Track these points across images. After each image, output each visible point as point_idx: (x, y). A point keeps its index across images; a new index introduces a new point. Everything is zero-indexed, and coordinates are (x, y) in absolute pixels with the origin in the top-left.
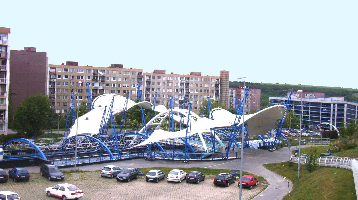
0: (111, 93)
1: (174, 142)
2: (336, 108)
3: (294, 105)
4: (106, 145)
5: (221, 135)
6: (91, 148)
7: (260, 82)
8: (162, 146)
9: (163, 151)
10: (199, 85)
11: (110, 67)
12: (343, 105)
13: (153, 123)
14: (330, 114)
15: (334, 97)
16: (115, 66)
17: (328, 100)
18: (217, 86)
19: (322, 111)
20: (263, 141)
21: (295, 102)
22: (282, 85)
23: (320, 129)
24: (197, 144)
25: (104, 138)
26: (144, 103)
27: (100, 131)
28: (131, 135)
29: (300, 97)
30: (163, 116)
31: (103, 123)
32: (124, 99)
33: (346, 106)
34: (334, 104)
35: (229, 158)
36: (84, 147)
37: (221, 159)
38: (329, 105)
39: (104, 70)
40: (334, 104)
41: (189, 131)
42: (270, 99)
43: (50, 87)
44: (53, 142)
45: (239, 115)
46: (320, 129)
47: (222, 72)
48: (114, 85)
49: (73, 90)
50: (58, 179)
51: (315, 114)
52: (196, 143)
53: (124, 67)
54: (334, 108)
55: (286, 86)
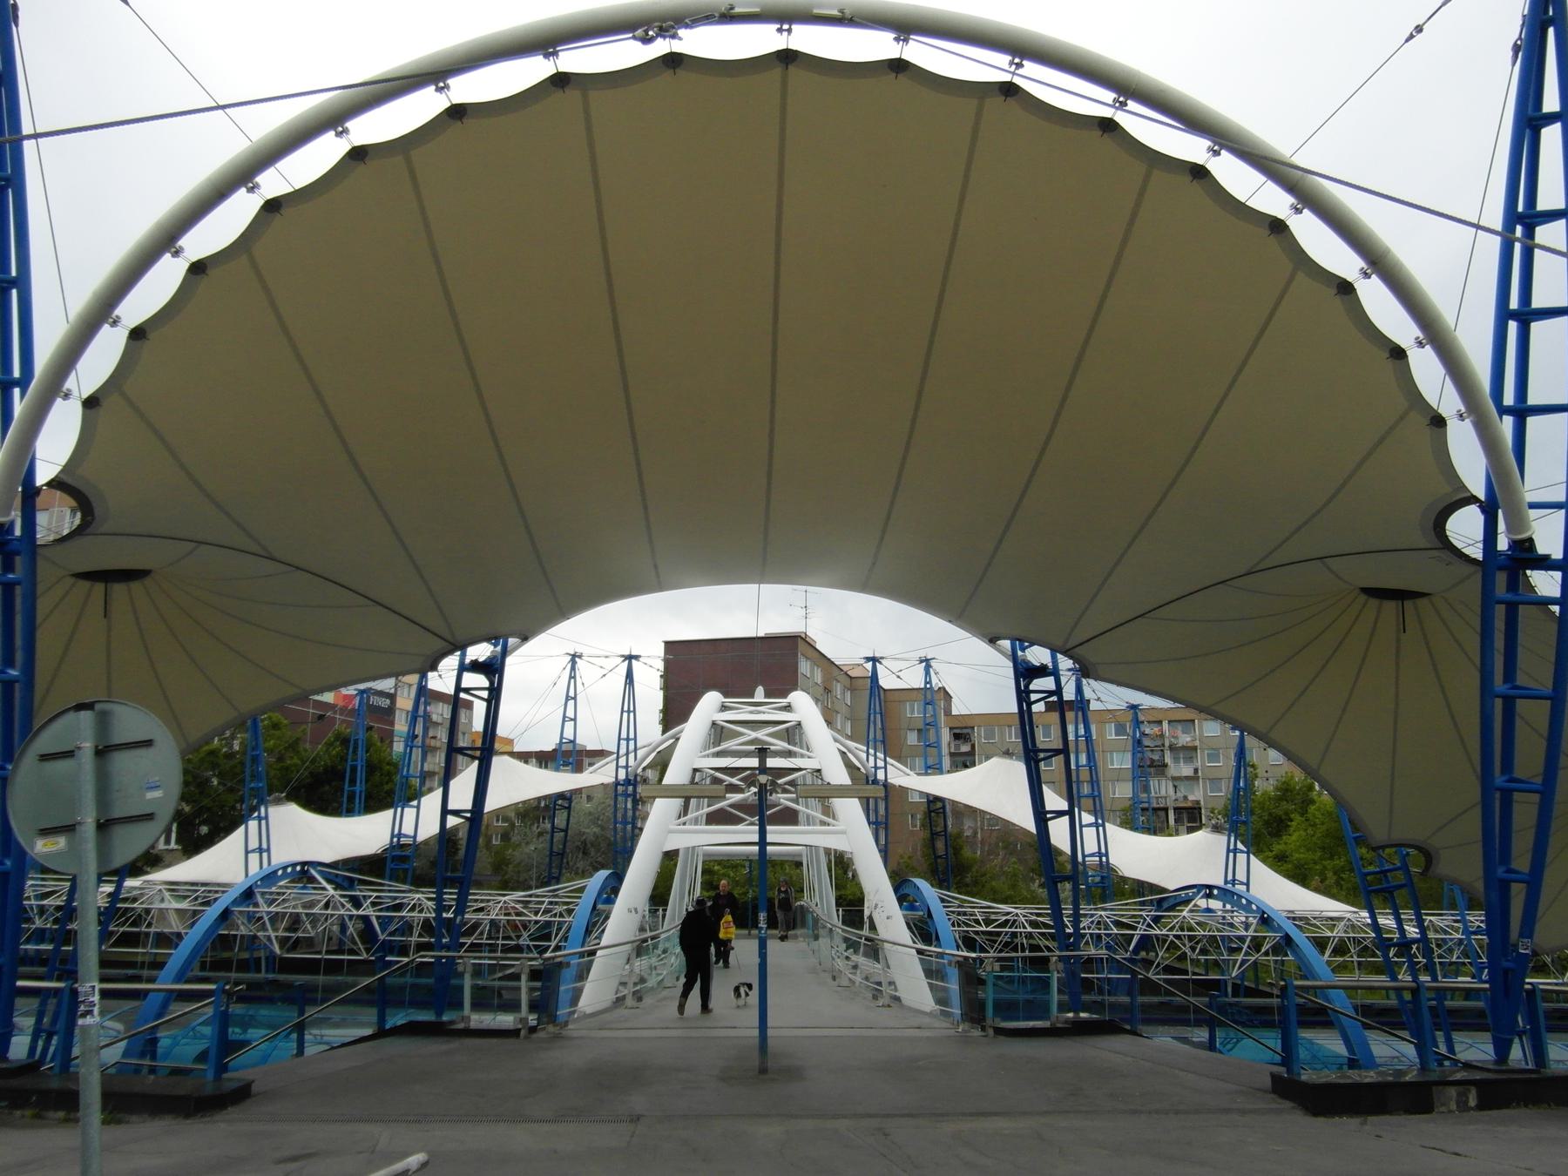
8: (576, 981)
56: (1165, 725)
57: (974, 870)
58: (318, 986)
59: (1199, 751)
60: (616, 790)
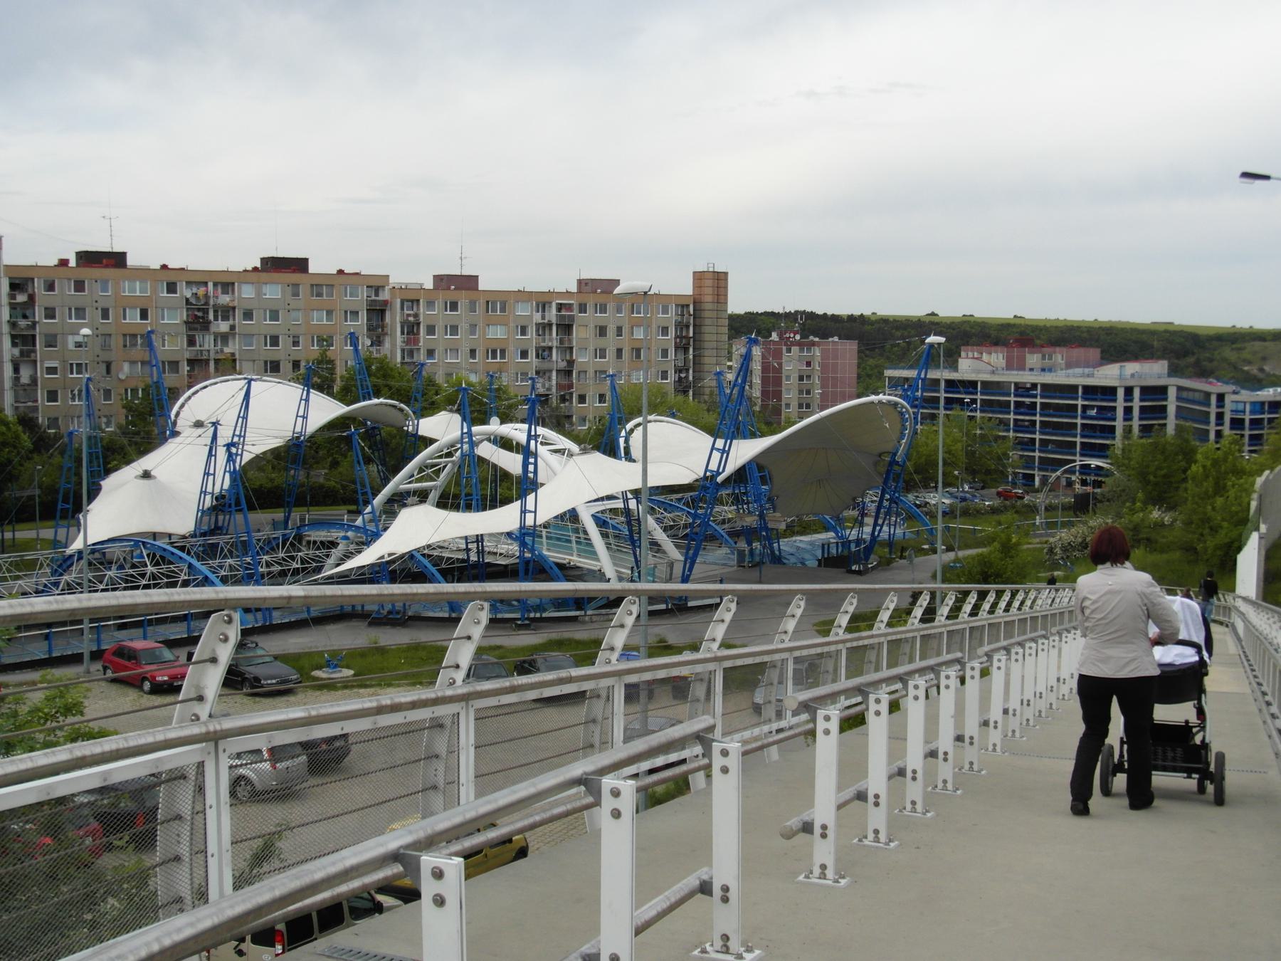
0: (266, 371)
1: (481, 552)
2: (1136, 404)
3: (979, 397)
5: (674, 521)
7: (867, 312)
8: (440, 571)
10: (611, 331)
11: (255, 269)
12: (1162, 391)
13: (410, 483)
14: (1114, 427)
15: (1127, 360)
16: (274, 265)
17: (1109, 375)
18: (682, 326)
19: (1083, 418)
20: (837, 534)
21: (985, 384)
23: (1077, 486)
24: (579, 556)
25: (215, 546)
26: (376, 405)
27: (198, 522)
29: (1009, 366)
30: (449, 455)
31: (209, 489)
32: (295, 391)
33: (1172, 393)
34: (1129, 391)
35: (690, 604)
37: (663, 607)
38: (1110, 392)
39: (233, 284)
40: (1129, 391)
41: (530, 506)
42: (889, 378)
44: (9, 571)
45: (723, 441)
46: (1077, 486)
47: (699, 277)
48: (275, 341)
50: (175, 684)
51: (1057, 427)
52: (575, 553)
53: (312, 269)
54: (1129, 404)
56: (210, 285)
57: (1199, 457)
58: (40, 519)
59: (237, 310)
60: (977, 358)
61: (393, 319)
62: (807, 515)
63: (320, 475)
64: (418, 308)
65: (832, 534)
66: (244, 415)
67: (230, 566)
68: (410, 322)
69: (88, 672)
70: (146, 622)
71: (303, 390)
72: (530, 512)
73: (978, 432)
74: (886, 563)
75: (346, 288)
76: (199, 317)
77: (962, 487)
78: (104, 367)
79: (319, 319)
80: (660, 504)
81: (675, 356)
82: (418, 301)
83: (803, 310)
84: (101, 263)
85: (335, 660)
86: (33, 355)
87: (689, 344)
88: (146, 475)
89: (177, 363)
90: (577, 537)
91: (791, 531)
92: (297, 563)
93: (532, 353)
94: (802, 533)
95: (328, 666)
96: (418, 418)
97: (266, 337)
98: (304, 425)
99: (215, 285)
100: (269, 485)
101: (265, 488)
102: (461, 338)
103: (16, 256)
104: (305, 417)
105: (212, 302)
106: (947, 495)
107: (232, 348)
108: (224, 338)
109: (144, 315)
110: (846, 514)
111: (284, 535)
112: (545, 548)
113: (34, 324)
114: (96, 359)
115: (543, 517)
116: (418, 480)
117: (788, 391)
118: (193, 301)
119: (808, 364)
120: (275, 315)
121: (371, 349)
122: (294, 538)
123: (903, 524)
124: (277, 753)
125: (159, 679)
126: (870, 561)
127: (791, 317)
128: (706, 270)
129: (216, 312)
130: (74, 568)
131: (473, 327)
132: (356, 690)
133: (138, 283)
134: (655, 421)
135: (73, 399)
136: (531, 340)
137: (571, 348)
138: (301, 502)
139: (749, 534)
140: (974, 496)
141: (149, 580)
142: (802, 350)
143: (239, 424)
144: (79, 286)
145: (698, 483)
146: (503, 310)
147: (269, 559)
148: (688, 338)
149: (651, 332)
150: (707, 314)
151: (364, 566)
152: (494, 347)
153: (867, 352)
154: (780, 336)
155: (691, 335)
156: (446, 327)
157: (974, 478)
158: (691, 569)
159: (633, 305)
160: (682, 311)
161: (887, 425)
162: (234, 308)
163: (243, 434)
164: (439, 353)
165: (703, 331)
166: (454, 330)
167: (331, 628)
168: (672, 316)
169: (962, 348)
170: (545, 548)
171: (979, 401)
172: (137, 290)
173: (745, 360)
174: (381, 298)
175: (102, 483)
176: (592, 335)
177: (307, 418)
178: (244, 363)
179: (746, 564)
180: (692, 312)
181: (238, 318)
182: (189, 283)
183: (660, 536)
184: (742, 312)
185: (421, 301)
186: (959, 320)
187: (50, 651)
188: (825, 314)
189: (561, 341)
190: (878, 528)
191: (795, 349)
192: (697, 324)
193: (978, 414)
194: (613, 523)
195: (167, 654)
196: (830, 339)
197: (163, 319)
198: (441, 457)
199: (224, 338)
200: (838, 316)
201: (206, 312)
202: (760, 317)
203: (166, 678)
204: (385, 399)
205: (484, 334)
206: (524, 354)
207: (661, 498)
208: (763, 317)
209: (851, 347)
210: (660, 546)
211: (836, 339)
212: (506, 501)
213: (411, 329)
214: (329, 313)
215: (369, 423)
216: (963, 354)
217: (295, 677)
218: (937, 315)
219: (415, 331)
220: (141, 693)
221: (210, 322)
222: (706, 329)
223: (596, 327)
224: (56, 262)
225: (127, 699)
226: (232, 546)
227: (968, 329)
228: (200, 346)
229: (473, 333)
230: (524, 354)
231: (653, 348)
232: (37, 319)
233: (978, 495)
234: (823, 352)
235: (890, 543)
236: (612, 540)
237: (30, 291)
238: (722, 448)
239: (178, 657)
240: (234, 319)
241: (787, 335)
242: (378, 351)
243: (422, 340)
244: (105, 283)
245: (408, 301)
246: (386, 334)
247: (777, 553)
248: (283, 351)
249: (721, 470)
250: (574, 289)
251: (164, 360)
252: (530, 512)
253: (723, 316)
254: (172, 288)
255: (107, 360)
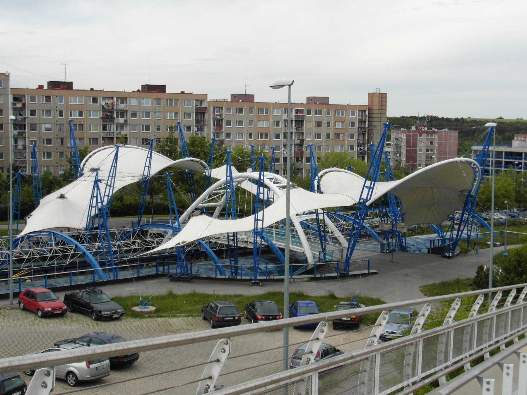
4: (88, 250)
6: (120, 251)
7: (465, 117)
8: (215, 252)
9: (215, 262)
10: (324, 125)
11: (139, 91)
16: (148, 89)
18: (362, 122)
22: (509, 122)
28: (156, 229)
35: (351, 273)
36: (126, 248)
37: (335, 274)
39: (126, 98)
42: (474, 150)
43: (14, 135)
45: (370, 182)
47: (371, 96)
48: (147, 128)
49: (62, 139)
50: (55, 313)
53: (168, 91)
55: (517, 122)
56: (115, 99)
61: (209, 117)
62: (423, 224)
63: (158, 199)
64: (222, 112)
65: (436, 235)
66: (114, 166)
67: (157, 242)
68: (218, 119)
69: (12, 304)
70: (71, 274)
71: (149, 151)
72: (260, 220)
73: (522, 180)
74: (464, 252)
75: (185, 101)
76: (109, 116)
77: (513, 210)
78: (60, 141)
79: (171, 117)
80: (341, 217)
81: (358, 138)
82: (222, 108)
83: (431, 115)
84: (60, 88)
85: (145, 301)
86: (24, 134)
87: (365, 131)
88: (62, 197)
89: (97, 139)
90: (293, 234)
91: (414, 232)
92: (154, 244)
93: (282, 135)
94: (422, 234)
95: (142, 304)
96: (211, 169)
97: (143, 126)
98: (149, 171)
99: (117, 99)
100: (135, 203)
101: (132, 204)
102: (322, 140)
103: (15, 83)
104: (149, 167)
105: (115, 108)
106: (504, 214)
107: (126, 131)
108: (122, 126)
109: (81, 114)
110: (444, 224)
111: (134, 230)
112: (275, 239)
113: (25, 118)
114: (56, 137)
115: (267, 224)
116: (208, 202)
117: (420, 158)
118: (106, 107)
119: (431, 143)
120: (148, 115)
121: (197, 132)
122: (139, 231)
123: (478, 230)
124: (90, 360)
125: (46, 309)
126: (456, 250)
127: (422, 119)
128: (375, 92)
129: (117, 113)
130: (19, 246)
131: (251, 122)
132: (155, 319)
133: (78, 97)
134: (335, 171)
135: (44, 157)
136: (281, 128)
137: (303, 133)
138: (147, 212)
139: (385, 234)
140: (519, 215)
141: (97, 250)
142: (428, 136)
143: (112, 170)
144: (48, 99)
145: (356, 206)
146: (267, 113)
147: (158, 240)
148: (364, 128)
149: (345, 125)
150: (375, 116)
151: (173, 248)
152: (262, 132)
153: (465, 138)
154: (417, 128)
155: (367, 126)
156: (237, 121)
157: (519, 205)
158: (351, 254)
159: (336, 111)
160: (362, 114)
161: (465, 174)
162: (127, 111)
163: (114, 175)
164: (233, 135)
165: (373, 125)
166: (241, 123)
167: (150, 282)
168: (356, 117)
169: (515, 135)
170: (275, 239)
171: (523, 164)
172: (75, 101)
173: (383, 136)
174: (203, 106)
175: (41, 200)
176: (314, 127)
177: (150, 167)
178: (131, 139)
179: (385, 251)
180: (367, 114)
181: (129, 116)
182: (104, 98)
183: (338, 234)
184: (399, 117)
185: (224, 108)
186: (515, 121)
187: (71, 282)
188: (443, 118)
189: (297, 129)
190: (460, 233)
191: (424, 135)
192: (370, 121)
193: (523, 170)
194: (313, 227)
195: (53, 295)
196: (443, 130)
197: (90, 116)
198: (220, 189)
199: (122, 126)
200: (450, 119)
201: (112, 112)
202: (408, 119)
203: (50, 309)
204: (193, 157)
205: (257, 125)
206: (278, 136)
207: (342, 214)
208: (410, 119)
209: (455, 134)
210: (338, 240)
211: (446, 130)
212: (248, 215)
213: (218, 122)
214: (176, 114)
215: (187, 171)
216: (515, 138)
217: (121, 310)
218: (503, 118)
219: (220, 123)
220: (37, 317)
221: (114, 118)
222: (375, 124)
223: (316, 122)
224: (37, 87)
225: (28, 320)
226: (122, 234)
227: (519, 126)
228: (109, 130)
229: (251, 125)
230: (278, 136)
231: (346, 134)
232: (26, 116)
233: (521, 214)
234: (439, 137)
235: (468, 240)
236: (311, 236)
237: (23, 102)
238: (369, 186)
239: (59, 298)
240: (127, 117)
241: (420, 128)
242: (201, 134)
243: (224, 128)
244: (61, 97)
245: (217, 108)
246: (205, 125)
247: (404, 245)
248: (152, 134)
249: (368, 199)
250: (305, 101)
251: (90, 137)
252: (260, 220)
253: (384, 117)
254: (95, 100)
255: (62, 137)
